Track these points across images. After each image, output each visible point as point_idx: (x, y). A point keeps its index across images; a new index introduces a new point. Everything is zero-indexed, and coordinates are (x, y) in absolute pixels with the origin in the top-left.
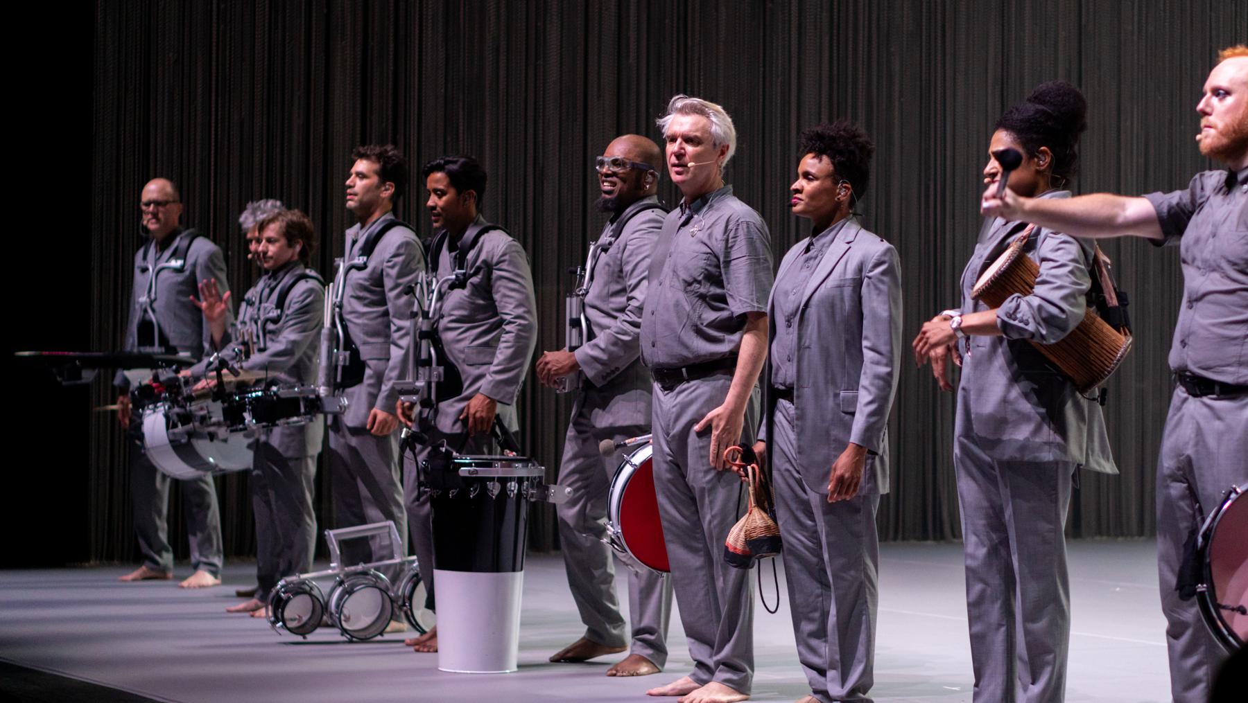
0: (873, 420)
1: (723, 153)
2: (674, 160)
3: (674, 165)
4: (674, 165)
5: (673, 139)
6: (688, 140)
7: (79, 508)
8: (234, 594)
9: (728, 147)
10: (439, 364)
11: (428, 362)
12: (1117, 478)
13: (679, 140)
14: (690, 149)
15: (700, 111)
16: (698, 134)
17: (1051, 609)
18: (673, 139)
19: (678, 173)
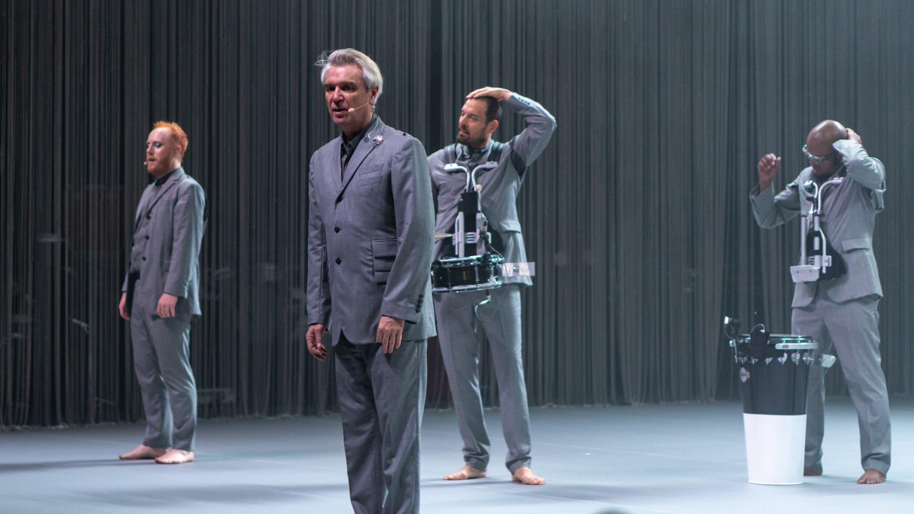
0: (187, 417)
1: (374, 94)
2: (333, 105)
3: (335, 110)
4: (335, 110)
5: (331, 88)
6: (346, 86)
7: (76, 386)
8: (117, 458)
9: (377, 88)
10: (827, 254)
11: (820, 252)
12: (815, 167)
13: (337, 89)
14: (347, 94)
15: (350, 61)
16: (353, 81)
17: (885, 438)
18: (331, 88)
19: (339, 117)
